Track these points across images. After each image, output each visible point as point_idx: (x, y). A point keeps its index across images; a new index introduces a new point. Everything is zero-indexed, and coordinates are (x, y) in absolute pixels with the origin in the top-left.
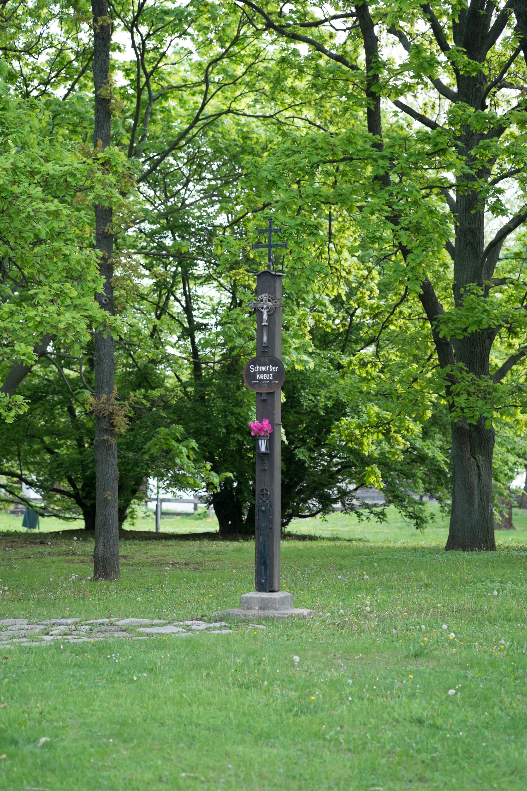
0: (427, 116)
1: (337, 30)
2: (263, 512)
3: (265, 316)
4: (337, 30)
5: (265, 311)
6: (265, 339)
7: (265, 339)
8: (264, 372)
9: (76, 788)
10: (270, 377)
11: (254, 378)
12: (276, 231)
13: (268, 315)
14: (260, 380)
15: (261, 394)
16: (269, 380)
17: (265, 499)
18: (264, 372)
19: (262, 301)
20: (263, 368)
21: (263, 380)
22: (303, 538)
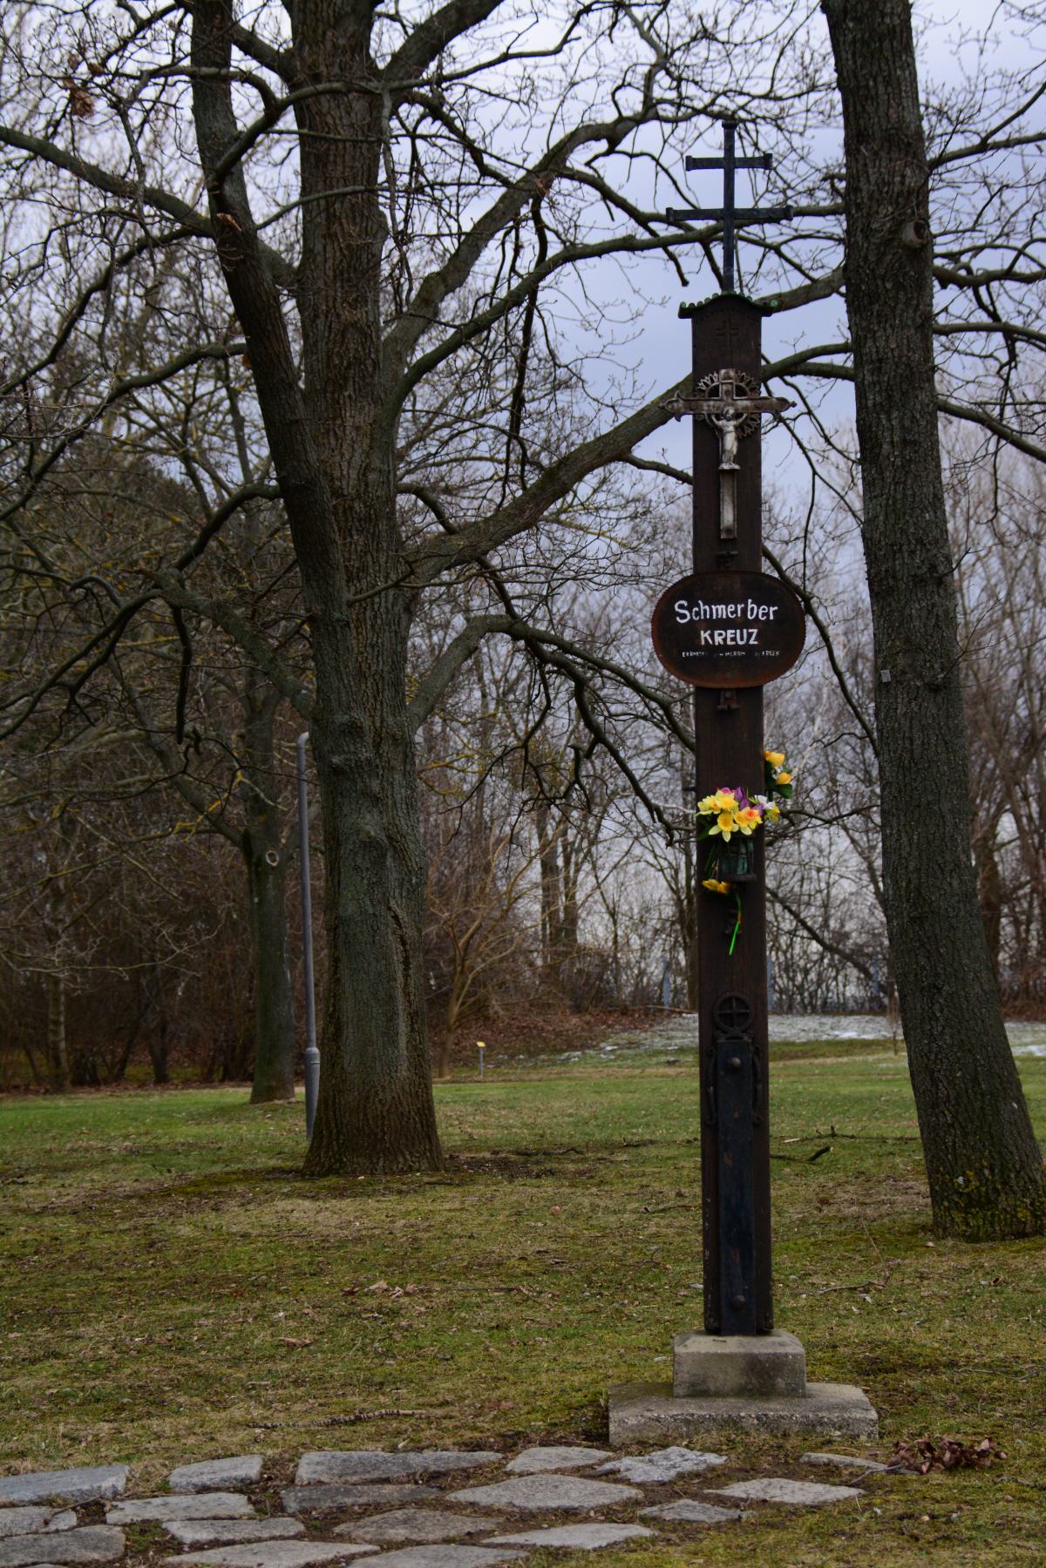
0: (830, 49)
1: (558, 51)
2: (734, 1070)
3: (730, 442)
4: (558, 51)
5: (730, 426)
6: (728, 516)
7: (728, 516)
8: (725, 624)
9: (863, 1561)
10: (752, 637)
11: (693, 642)
12: (748, 163)
13: (738, 439)
14: (712, 649)
15: (717, 692)
16: (747, 647)
17: (736, 1031)
18: (725, 624)
19: (715, 392)
20: (721, 611)
21: (724, 647)
22: (521, 1162)
